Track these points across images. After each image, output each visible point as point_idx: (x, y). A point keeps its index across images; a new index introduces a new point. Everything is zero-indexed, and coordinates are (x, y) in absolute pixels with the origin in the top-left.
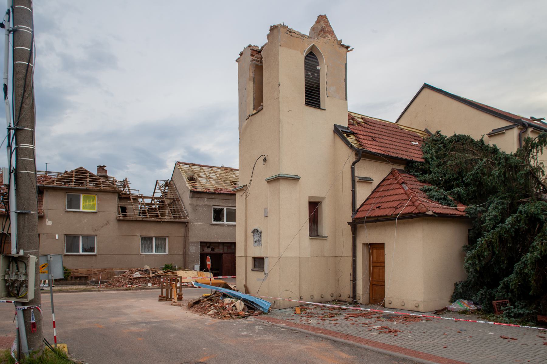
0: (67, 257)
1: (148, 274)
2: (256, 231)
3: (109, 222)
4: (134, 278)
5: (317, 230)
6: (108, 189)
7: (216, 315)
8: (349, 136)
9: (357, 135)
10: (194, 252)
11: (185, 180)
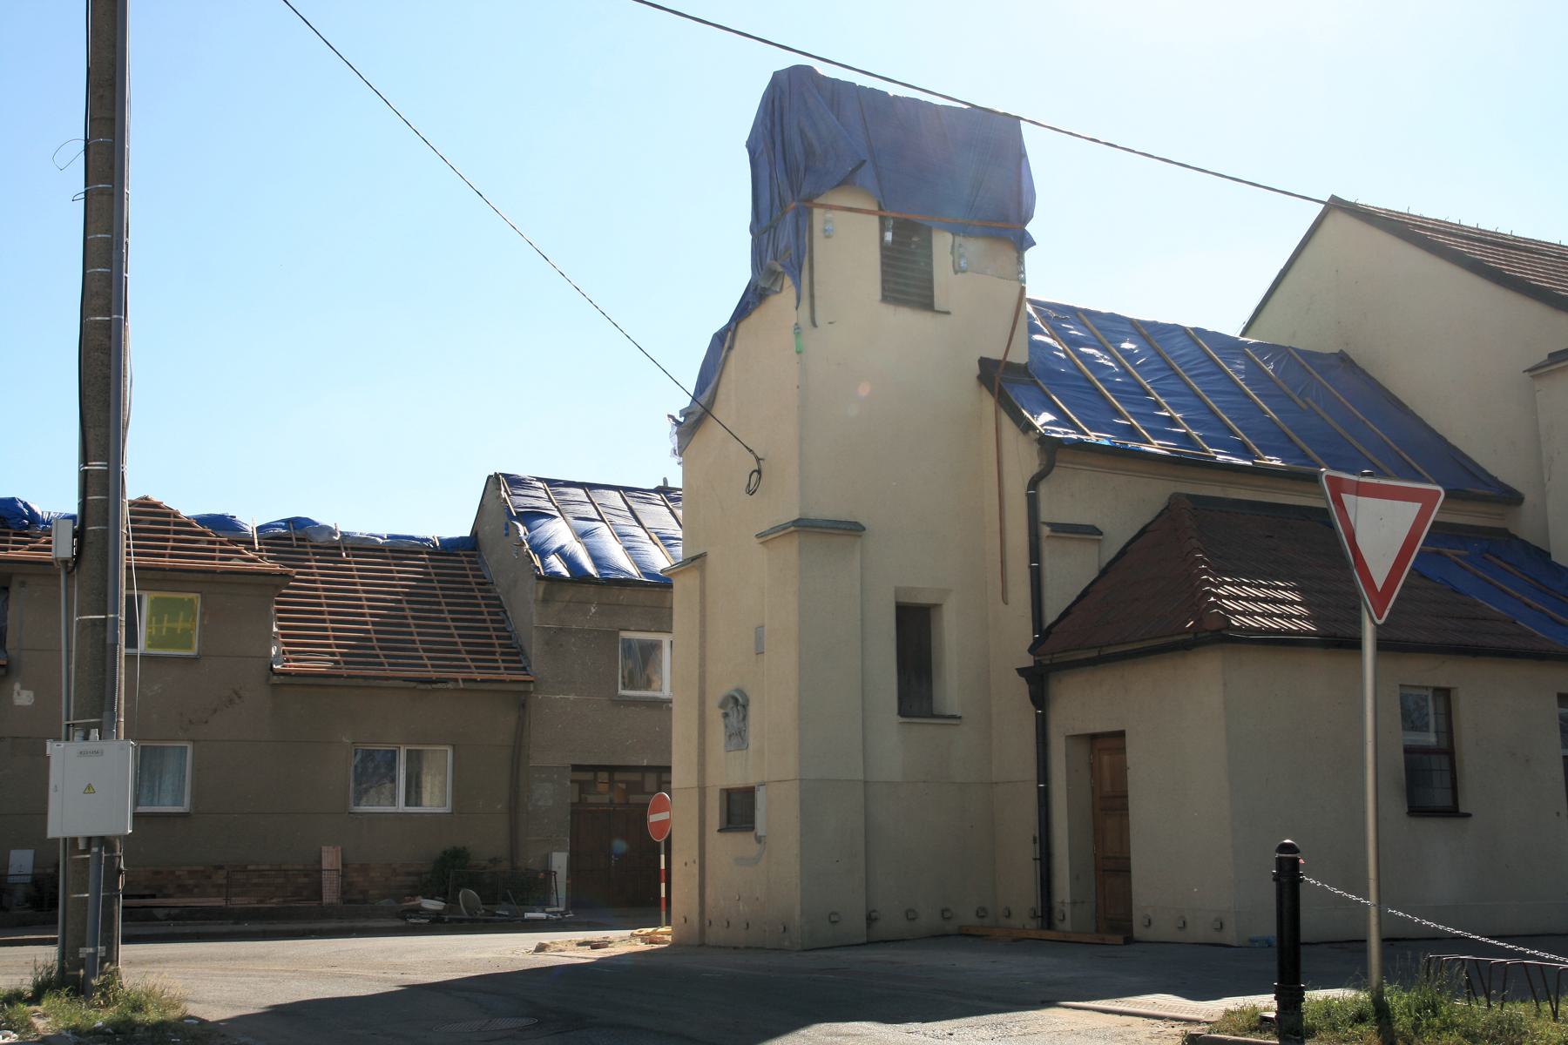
5: (930, 698)
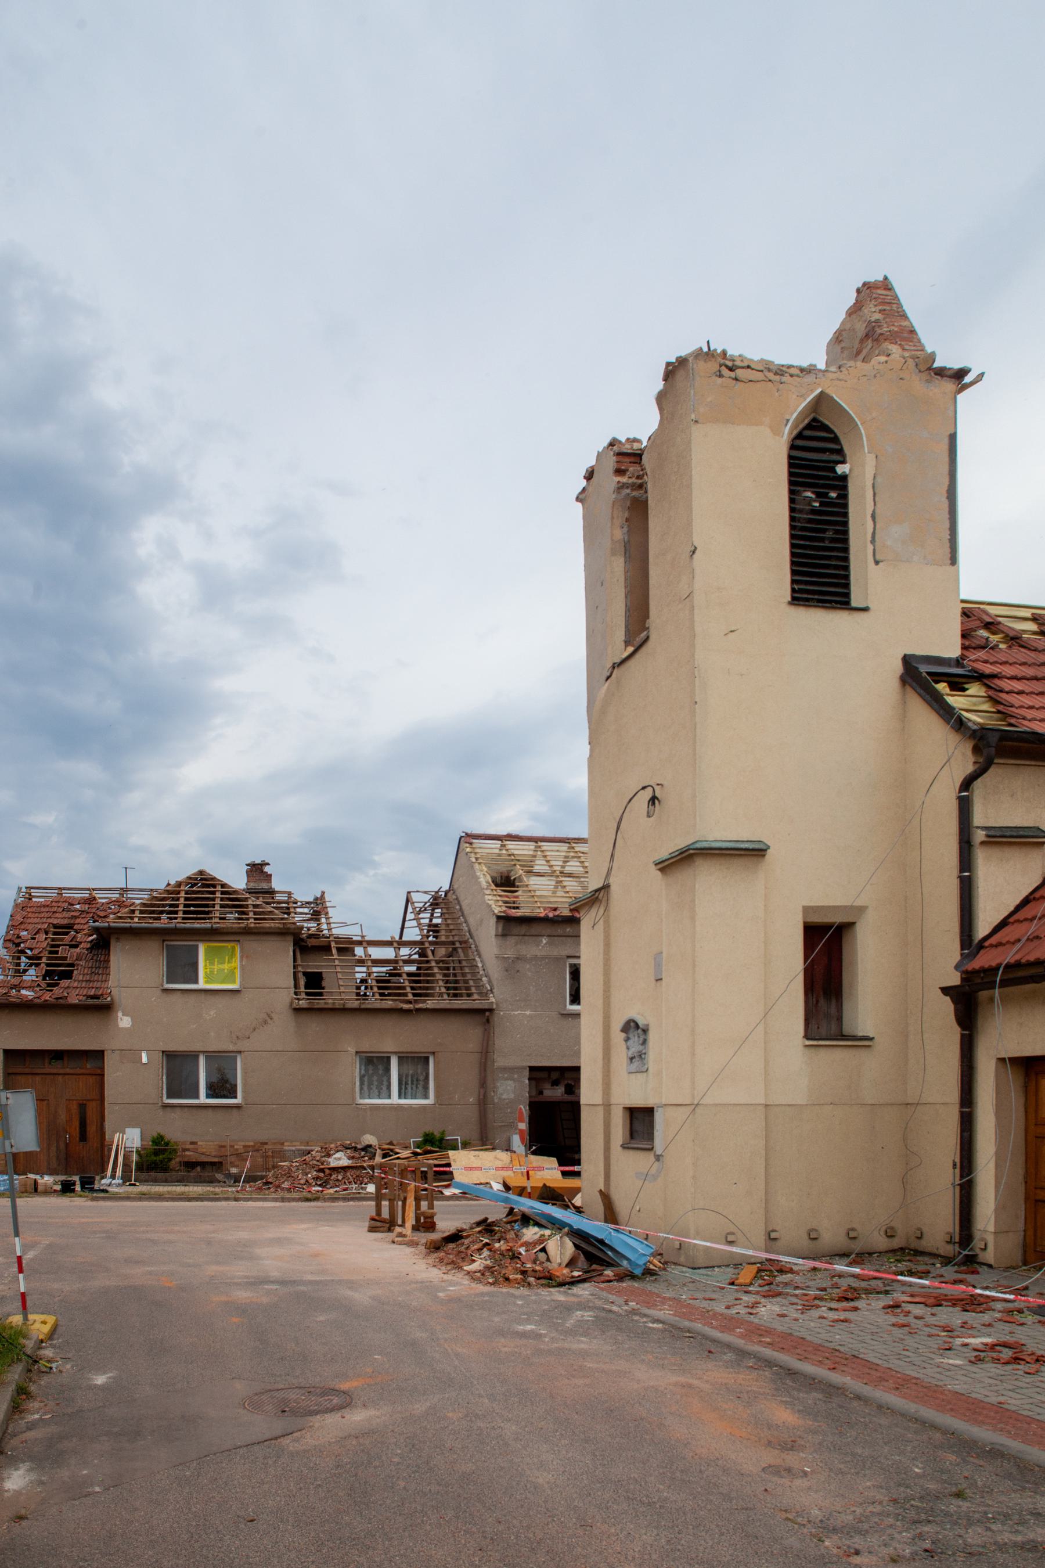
0: (169, 1109)
1: (370, 1159)
2: (631, 1027)
3: (273, 1015)
4: (330, 1169)
5: (840, 1019)
6: (267, 924)
7: (494, 1274)
8: (964, 690)
9: (997, 681)
10: (512, 1096)
11: (484, 884)
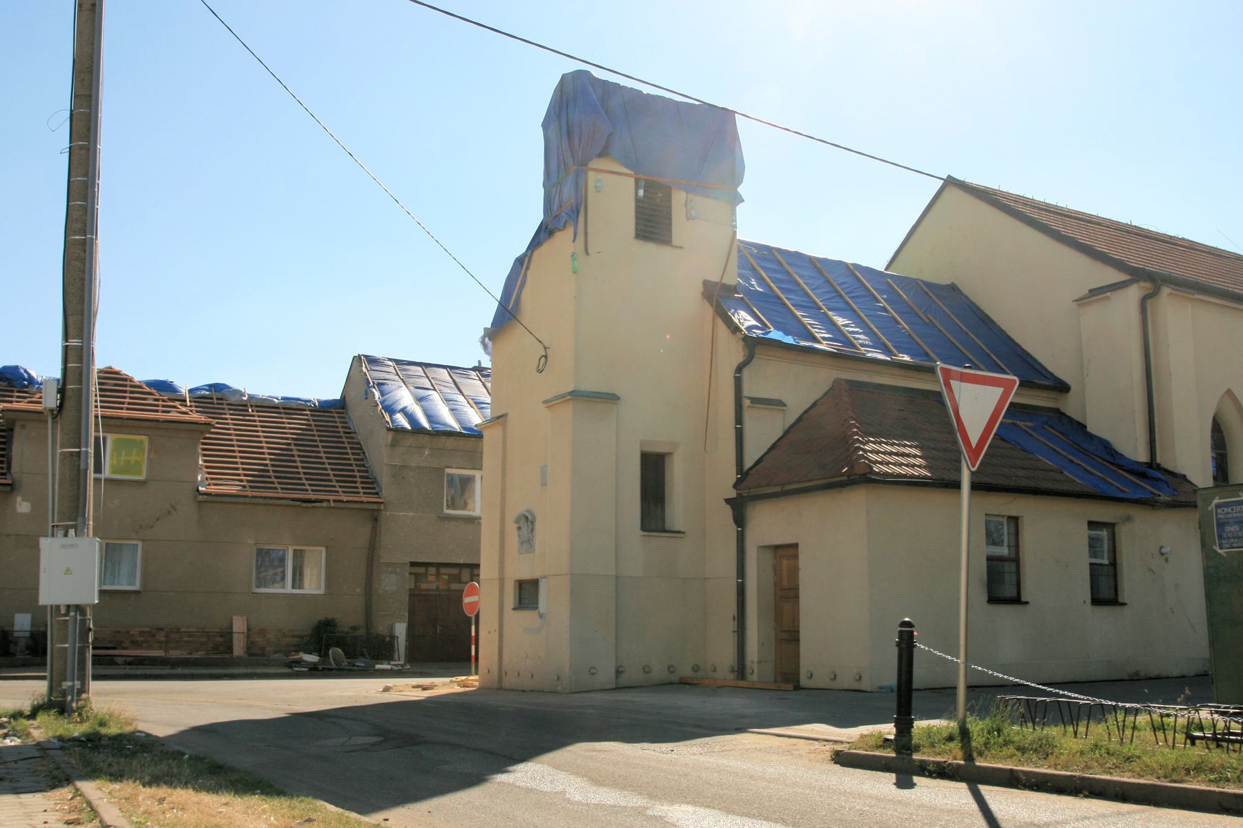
10: (394, 588)
